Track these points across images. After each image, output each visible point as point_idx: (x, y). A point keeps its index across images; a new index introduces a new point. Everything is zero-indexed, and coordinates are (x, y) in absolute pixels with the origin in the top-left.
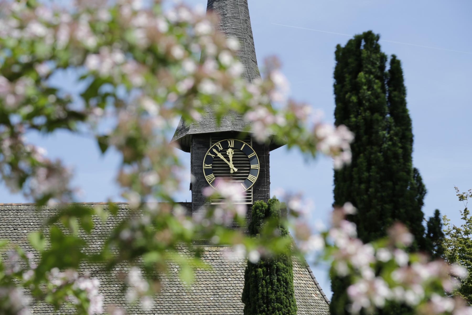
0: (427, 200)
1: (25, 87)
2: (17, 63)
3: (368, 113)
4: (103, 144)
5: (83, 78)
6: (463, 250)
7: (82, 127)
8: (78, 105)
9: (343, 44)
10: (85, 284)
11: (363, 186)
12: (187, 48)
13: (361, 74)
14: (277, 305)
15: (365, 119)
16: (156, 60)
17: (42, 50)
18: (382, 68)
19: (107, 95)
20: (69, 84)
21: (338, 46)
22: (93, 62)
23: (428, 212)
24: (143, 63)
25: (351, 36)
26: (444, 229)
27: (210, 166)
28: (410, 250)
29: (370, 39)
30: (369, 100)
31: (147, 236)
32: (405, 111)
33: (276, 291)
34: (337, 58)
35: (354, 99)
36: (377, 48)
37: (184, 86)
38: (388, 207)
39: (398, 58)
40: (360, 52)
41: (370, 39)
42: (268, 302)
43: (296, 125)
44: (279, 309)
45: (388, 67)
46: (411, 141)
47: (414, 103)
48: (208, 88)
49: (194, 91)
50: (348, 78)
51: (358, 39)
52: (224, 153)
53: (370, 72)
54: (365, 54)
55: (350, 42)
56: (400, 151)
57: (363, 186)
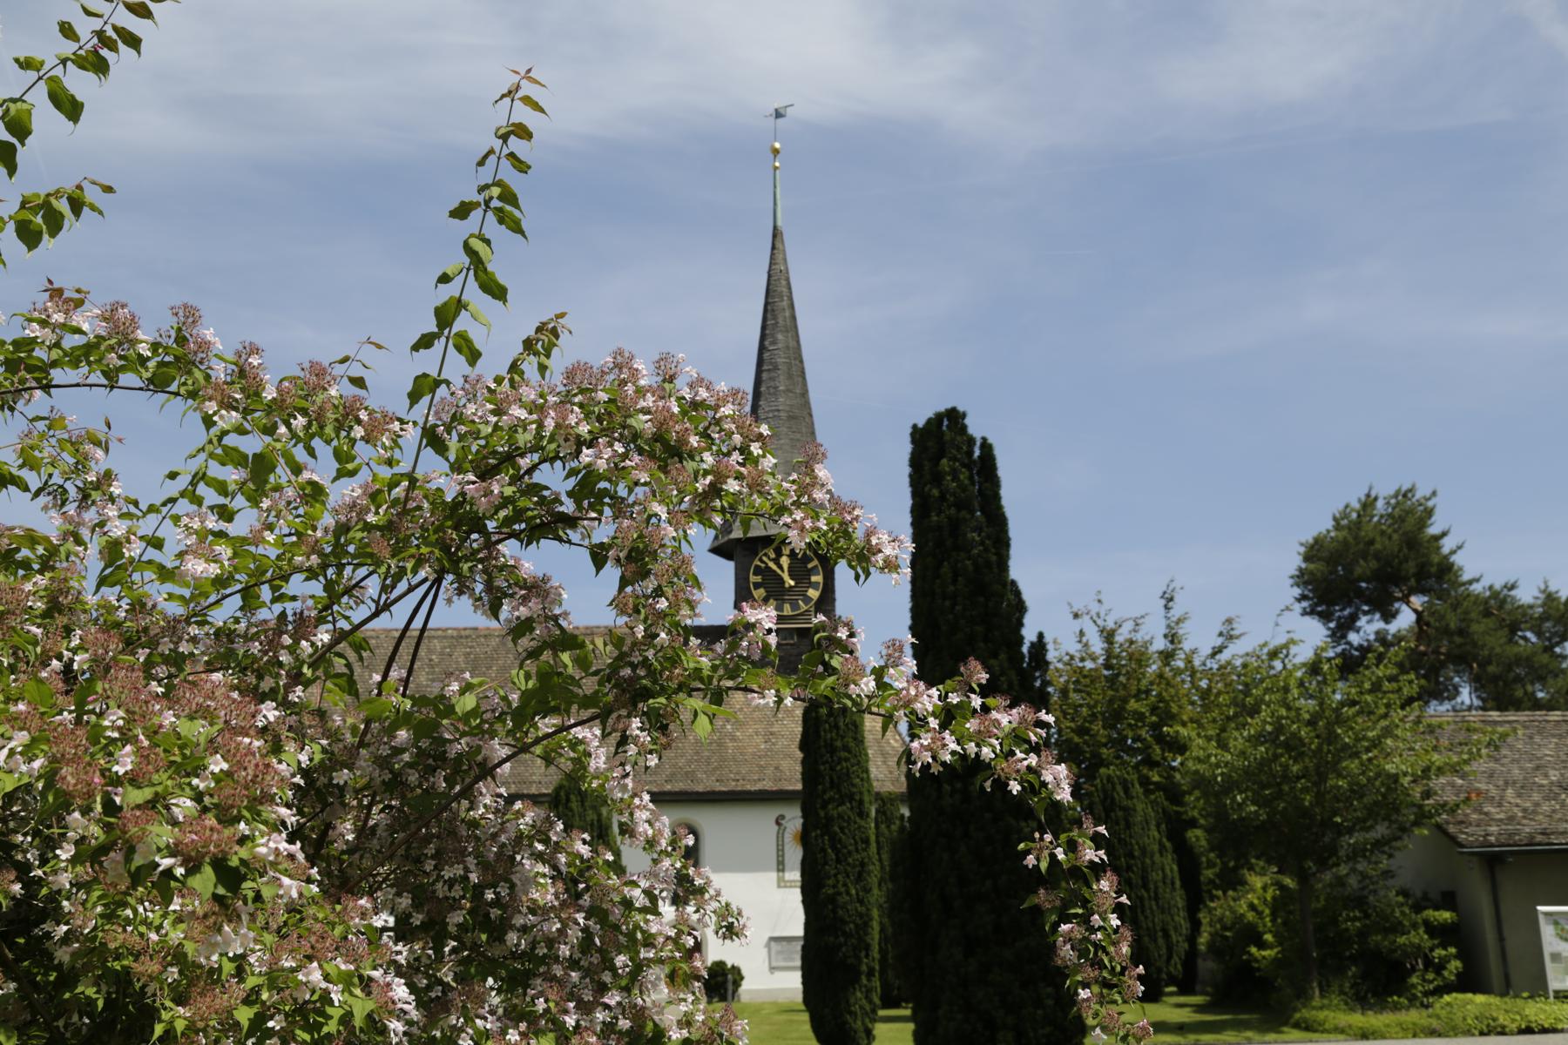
0: (1027, 620)
1: (500, 486)
2: (495, 453)
3: (953, 511)
4: (599, 556)
5: (573, 473)
6: (1077, 682)
7: (574, 536)
8: (568, 507)
9: (921, 423)
10: (580, 732)
11: (947, 603)
12: (705, 435)
13: (944, 461)
14: (844, 754)
15: (949, 518)
16: (667, 451)
17: (524, 438)
18: (971, 453)
19: (605, 492)
20: (554, 479)
21: (915, 426)
22: (587, 455)
23: (1029, 634)
24: (652, 456)
25: (930, 414)
26: (1051, 655)
27: (758, 579)
28: (985, 691)
29: (954, 417)
30: (954, 494)
31: (652, 673)
32: (1000, 507)
33: (843, 737)
34: (913, 441)
35: (935, 492)
36: (964, 427)
37: (702, 484)
38: (979, 629)
39: (990, 441)
40: (943, 433)
41: (954, 417)
42: (832, 750)
43: (845, 532)
44: (847, 760)
45: (977, 453)
46: (1008, 546)
47: (1012, 497)
48: (732, 486)
49: (715, 490)
50: (927, 465)
51: (939, 417)
52: (777, 561)
53: (955, 459)
54: (947, 437)
55: (929, 421)
56: (994, 558)
57: (947, 603)
